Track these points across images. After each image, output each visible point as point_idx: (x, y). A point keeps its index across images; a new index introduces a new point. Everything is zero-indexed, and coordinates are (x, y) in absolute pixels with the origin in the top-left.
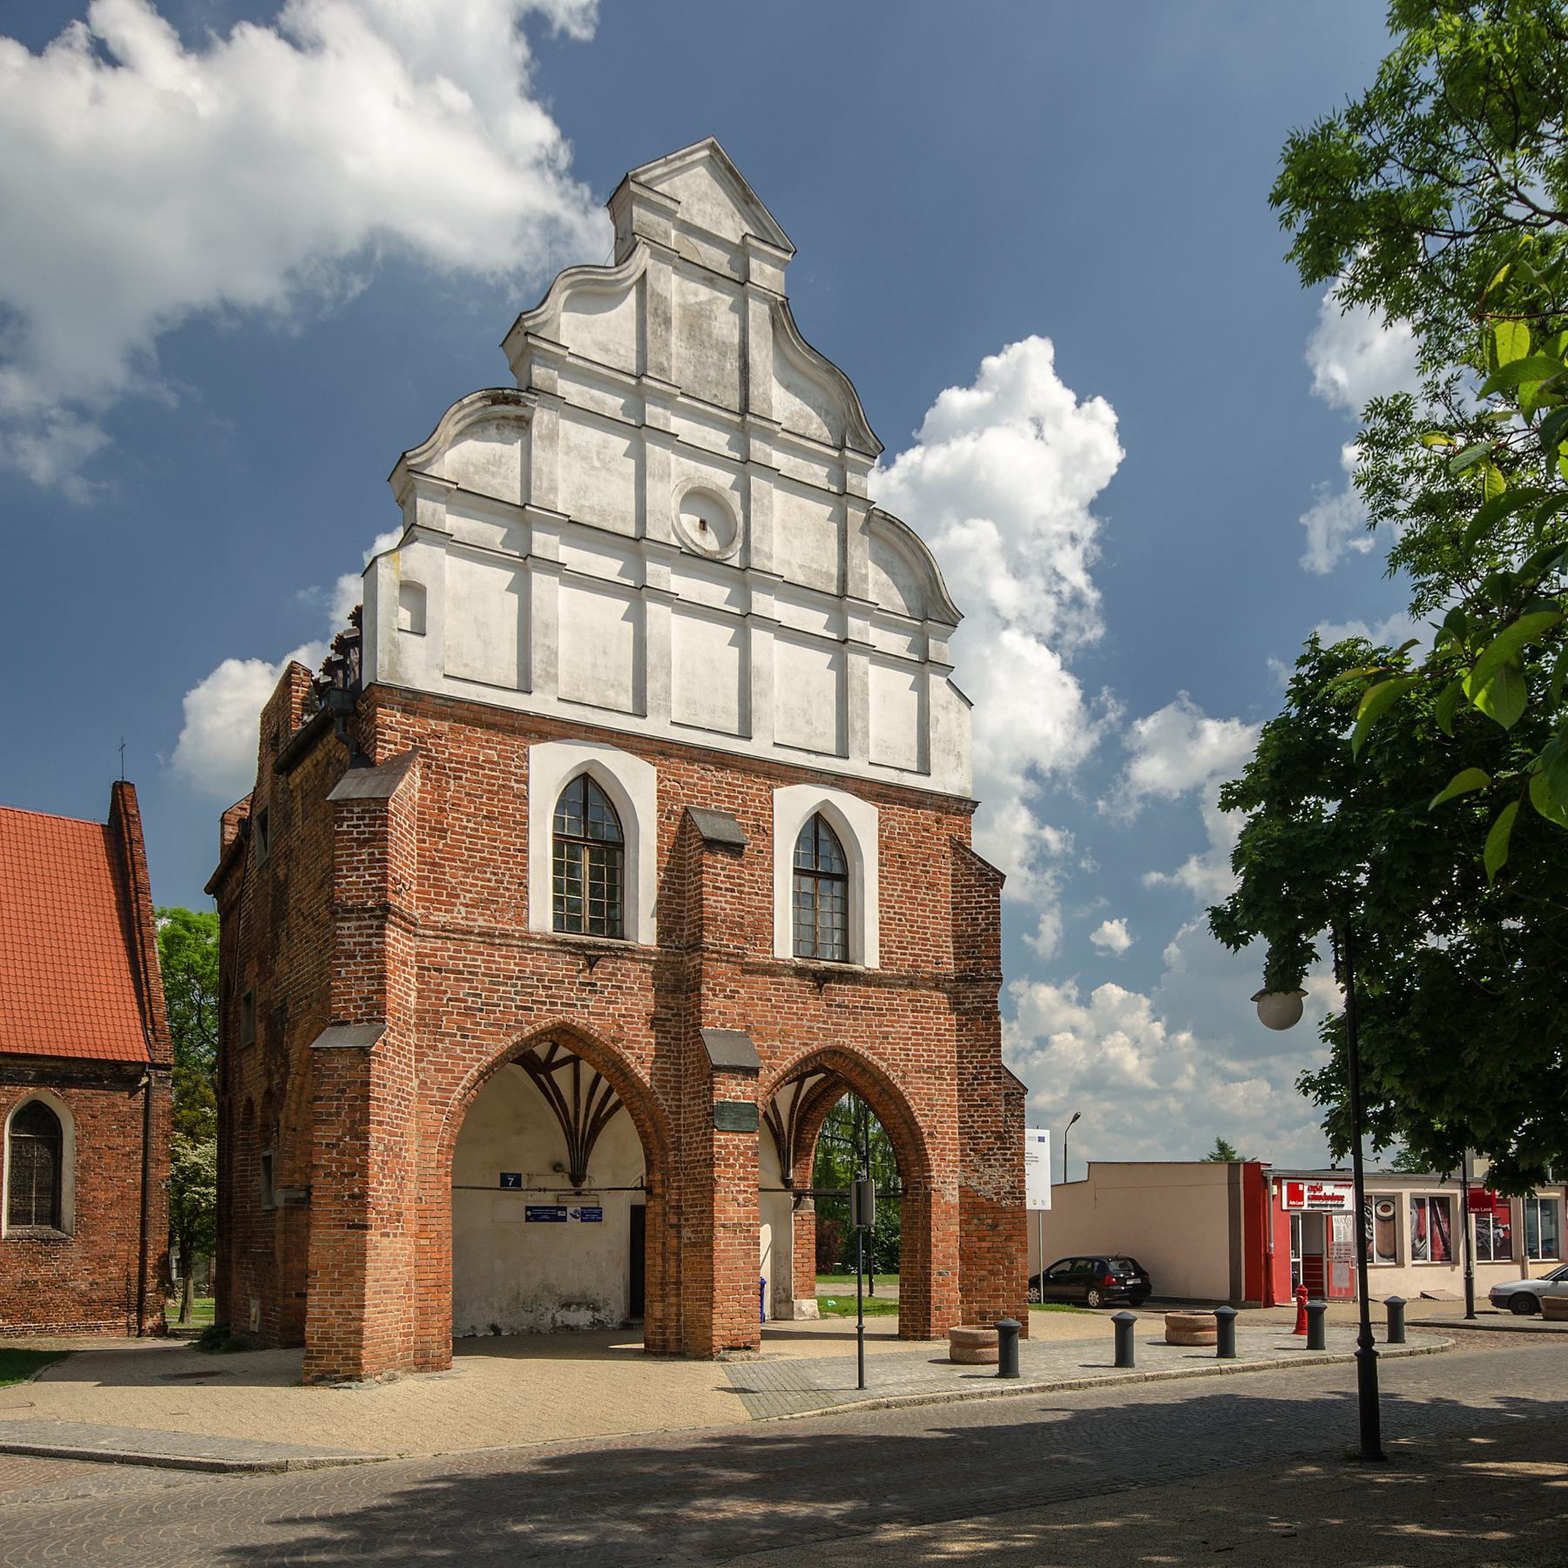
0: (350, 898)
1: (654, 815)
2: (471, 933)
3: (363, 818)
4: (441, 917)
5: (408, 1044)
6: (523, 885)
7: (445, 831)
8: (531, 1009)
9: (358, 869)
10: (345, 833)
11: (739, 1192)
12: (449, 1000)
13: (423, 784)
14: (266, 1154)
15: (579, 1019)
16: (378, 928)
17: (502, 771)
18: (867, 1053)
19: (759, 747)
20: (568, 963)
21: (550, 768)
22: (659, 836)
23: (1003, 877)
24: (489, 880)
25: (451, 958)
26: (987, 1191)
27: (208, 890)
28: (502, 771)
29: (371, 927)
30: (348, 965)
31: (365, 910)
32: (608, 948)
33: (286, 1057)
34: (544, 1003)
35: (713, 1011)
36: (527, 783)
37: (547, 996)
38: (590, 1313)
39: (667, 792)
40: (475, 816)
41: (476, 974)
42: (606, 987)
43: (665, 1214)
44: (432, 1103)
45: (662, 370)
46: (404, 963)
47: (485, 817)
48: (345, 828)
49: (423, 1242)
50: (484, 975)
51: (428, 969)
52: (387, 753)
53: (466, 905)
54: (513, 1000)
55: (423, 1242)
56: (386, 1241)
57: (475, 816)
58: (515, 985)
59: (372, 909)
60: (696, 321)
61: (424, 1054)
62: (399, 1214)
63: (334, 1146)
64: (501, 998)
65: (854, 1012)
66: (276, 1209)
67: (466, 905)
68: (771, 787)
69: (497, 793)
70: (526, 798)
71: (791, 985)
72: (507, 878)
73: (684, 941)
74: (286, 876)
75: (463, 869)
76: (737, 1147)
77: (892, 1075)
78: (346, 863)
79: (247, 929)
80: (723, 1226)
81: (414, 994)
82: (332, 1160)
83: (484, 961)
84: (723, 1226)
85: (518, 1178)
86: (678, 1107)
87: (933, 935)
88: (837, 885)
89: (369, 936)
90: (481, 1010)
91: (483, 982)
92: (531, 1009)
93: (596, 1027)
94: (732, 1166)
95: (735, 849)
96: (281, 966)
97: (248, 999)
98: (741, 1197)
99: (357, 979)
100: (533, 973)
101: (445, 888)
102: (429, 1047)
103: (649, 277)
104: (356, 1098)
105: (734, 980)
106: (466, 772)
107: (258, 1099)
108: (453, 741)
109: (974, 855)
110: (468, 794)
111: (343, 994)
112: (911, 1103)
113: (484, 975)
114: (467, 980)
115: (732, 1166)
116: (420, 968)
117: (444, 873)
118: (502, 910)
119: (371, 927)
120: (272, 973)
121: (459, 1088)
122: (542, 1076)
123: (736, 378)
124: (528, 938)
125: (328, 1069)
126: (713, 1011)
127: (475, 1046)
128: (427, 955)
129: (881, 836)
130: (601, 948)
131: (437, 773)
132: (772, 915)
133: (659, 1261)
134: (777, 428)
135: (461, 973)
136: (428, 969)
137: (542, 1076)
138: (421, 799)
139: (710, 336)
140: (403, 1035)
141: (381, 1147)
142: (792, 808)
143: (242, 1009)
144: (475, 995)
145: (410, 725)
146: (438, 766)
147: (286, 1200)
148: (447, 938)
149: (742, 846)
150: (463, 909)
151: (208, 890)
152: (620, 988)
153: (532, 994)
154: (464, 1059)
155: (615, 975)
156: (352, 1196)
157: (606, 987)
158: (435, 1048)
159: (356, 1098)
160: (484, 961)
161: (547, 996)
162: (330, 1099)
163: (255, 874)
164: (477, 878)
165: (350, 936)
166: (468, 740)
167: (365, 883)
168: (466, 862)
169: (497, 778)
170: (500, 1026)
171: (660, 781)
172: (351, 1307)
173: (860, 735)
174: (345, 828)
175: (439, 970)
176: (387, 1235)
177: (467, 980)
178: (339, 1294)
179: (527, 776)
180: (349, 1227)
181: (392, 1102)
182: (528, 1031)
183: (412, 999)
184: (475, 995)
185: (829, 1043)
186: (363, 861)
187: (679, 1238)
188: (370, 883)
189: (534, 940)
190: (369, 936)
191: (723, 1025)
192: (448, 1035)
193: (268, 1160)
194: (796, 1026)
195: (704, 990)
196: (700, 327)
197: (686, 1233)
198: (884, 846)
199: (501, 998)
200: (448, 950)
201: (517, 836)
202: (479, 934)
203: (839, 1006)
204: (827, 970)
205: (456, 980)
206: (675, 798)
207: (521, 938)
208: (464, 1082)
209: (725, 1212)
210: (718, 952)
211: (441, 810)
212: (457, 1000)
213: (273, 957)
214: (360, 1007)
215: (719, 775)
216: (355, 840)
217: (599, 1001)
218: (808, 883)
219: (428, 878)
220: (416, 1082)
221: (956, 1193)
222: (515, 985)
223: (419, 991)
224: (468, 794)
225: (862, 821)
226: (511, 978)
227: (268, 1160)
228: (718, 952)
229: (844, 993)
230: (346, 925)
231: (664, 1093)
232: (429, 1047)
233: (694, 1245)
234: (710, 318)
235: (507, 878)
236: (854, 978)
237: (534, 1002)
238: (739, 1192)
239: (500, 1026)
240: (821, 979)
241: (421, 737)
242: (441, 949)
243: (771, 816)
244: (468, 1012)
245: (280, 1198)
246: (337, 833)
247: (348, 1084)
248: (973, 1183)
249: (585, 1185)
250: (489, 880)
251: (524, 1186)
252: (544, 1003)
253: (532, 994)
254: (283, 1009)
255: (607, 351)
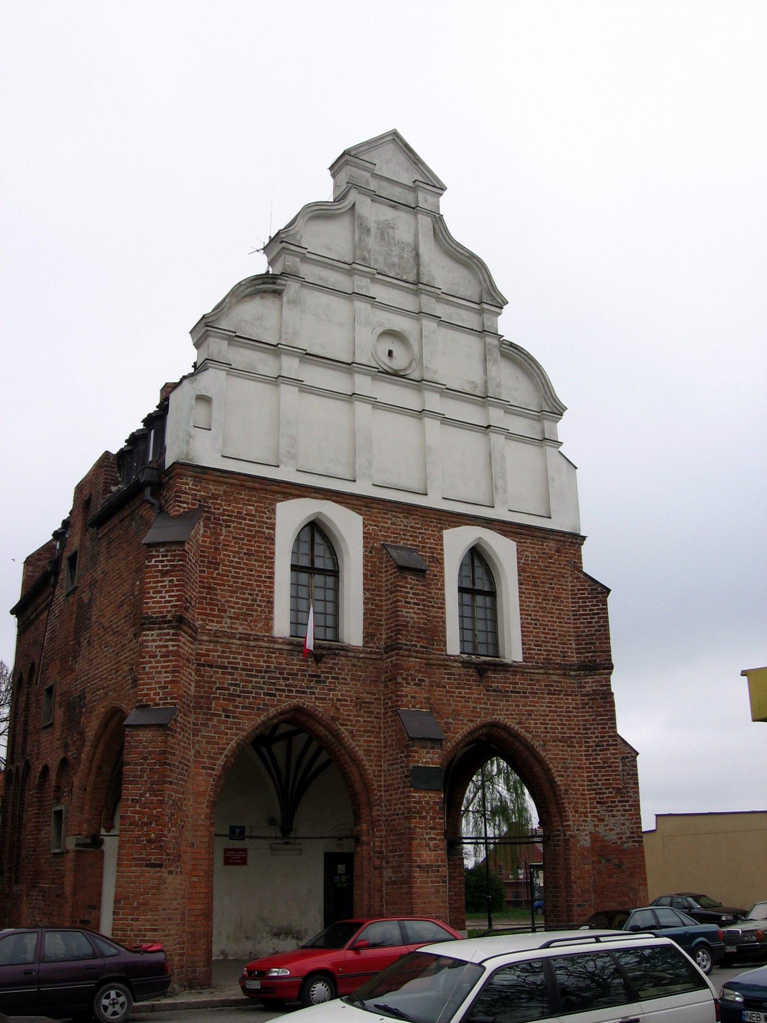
0: (155, 613)
1: (360, 550)
2: (234, 638)
3: (166, 556)
4: (213, 626)
5: (189, 722)
6: (270, 603)
7: (218, 564)
8: (275, 695)
9: (161, 592)
10: (153, 566)
11: (431, 839)
12: (218, 688)
13: (205, 531)
14: (58, 808)
15: (308, 702)
16: (174, 635)
17: (258, 521)
18: (517, 727)
19: (433, 501)
20: (301, 660)
21: (290, 517)
22: (364, 565)
23: (609, 591)
24: (247, 599)
25: (219, 657)
26: (612, 837)
27: (13, 612)
28: (258, 521)
29: (168, 634)
30: (150, 662)
31: (165, 622)
32: (329, 649)
33: (82, 733)
34: (283, 691)
35: (406, 696)
36: (274, 529)
37: (286, 685)
38: (294, 942)
39: (370, 534)
40: (239, 553)
41: (236, 669)
42: (328, 678)
43: (370, 859)
44: (203, 768)
45: (364, 259)
46: (189, 661)
47: (245, 554)
48: (153, 563)
49: (194, 879)
50: (242, 669)
51: (203, 665)
52: (182, 510)
53: (231, 618)
54: (262, 688)
55: (194, 879)
56: (171, 877)
57: (239, 553)
58: (263, 677)
59: (170, 621)
60: (385, 230)
61: (199, 731)
62: (180, 856)
63: (137, 801)
64: (253, 687)
65: (504, 694)
66: (68, 852)
67: (231, 618)
68: (442, 529)
69: (254, 537)
70: (273, 540)
71: (459, 675)
72: (259, 598)
73: (383, 643)
74: (90, 600)
75: (230, 591)
76: (427, 803)
77: (536, 744)
78: (152, 588)
79: (51, 639)
80: (419, 867)
81: (193, 684)
82: (135, 812)
83: (242, 659)
84: (419, 867)
85: (242, 830)
86: (380, 771)
87: (560, 635)
88: (488, 599)
89: (166, 641)
90: (239, 696)
91: (241, 675)
92: (275, 695)
93: (320, 708)
94: (425, 818)
95: (419, 572)
96: (81, 665)
97: (50, 691)
98: (432, 843)
99: (157, 673)
100: (276, 668)
101: (217, 605)
102: (202, 724)
103: (357, 206)
104: (155, 764)
105: (420, 672)
106: (233, 522)
107: (54, 767)
108: (226, 501)
109: (585, 574)
110: (234, 538)
111: (146, 684)
112: (551, 766)
113: (242, 669)
114: (230, 674)
115: (425, 818)
116: (198, 665)
117: (216, 595)
118: (255, 621)
119: (168, 634)
120: (73, 670)
121: (222, 757)
122: (264, 750)
123: (412, 262)
124: (273, 640)
125: (136, 741)
126: (406, 696)
127: (234, 723)
128: (203, 655)
129: (519, 563)
130: (324, 648)
131: (214, 523)
132: (444, 622)
133: (366, 897)
134: (439, 292)
135: (226, 668)
136: (203, 665)
137: (264, 750)
138: (204, 541)
139: (394, 238)
140: (186, 715)
141: (171, 802)
142: (456, 543)
143: (43, 698)
144: (236, 685)
145: (198, 491)
146: (215, 518)
147: (77, 845)
148: (217, 642)
149: (424, 571)
150: (228, 621)
151: (13, 612)
152: (337, 678)
153: (275, 684)
154: (227, 734)
155: (333, 668)
156: (150, 841)
157: (328, 678)
158: (206, 725)
159: (155, 764)
160: (242, 659)
161: (286, 685)
162: (136, 764)
163: (61, 598)
164: (238, 598)
165: (154, 641)
166: (235, 499)
167: (166, 602)
168: (231, 586)
169: (254, 526)
170: (253, 709)
171: (365, 526)
172: (146, 930)
173: (501, 491)
174: (153, 563)
175: (211, 666)
176: (613, 816)
177: (230, 674)
178: (137, 920)
179: (274, 524)
180: (147, 865)
181: (178, 767)
182: (272, 711)
183: (192, 688)
184: (236, 685)
185: (489, 719)
186: (164, 586)
187: (381, 877)
188: (169, 602)
189: (278, 643)
190: (166, 641)
191: (414, 707)
192: (215, 715)
193: (59, 814)
194: (464, 707)
195: (399, 680)
196: (388, 233)
197: (387, 874)
198: (521, 570)
199: (253, 687)
200: (217, 651)
201: (267, 567)
202: (240, 639)
203: (494, 691)
204: (485, 663)
205: (223, 673)
206: (376, 538)
207: (269, 641)
208: (226, 752)
209: (420, 855)
210: (409, 650)
211: (216, 549)
212: (222, 689)
213: (75, 657)
214: (158, 694)
215: (405, 521)
216: (159, 571)
217: (322, 689)
218: (467, 598)
219: (205, 598)
220: (193, 752)
221: (588, 838)
222: (263, 677)
223: (197, 682)
224: (234, 538)
225: (505, 552)
226: (260, 672)
227: (59, 814)
228: (409, 650)
229: (497, 680)
230: (150, 633)
231: (371, 761)
232: (202, 724)
233: (395, 883)
234: (394, 228)
235: (259, 598)
236: (505, 667)
237: (277, 690)
238: (431, 839)
239: (253, 709)
240: (482, 670)
241: (204, 498)
242: (212, 651)
243: (442, 550)
244: (231, 698)
245: (70, 843)
246: (148, 567)
247: (150, 753)
248: (601, 829)
249: (292, 835)
250: (247, 599)
251: (247, 834)
252: (283, 691)
253: (275, 684)
254: (82, 697)
255: (330, 250)
